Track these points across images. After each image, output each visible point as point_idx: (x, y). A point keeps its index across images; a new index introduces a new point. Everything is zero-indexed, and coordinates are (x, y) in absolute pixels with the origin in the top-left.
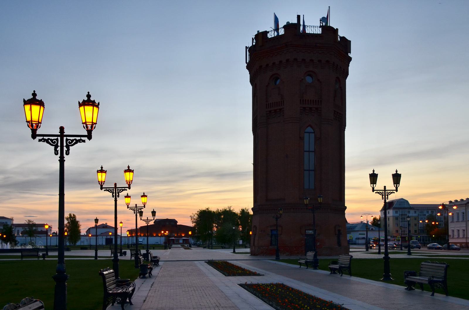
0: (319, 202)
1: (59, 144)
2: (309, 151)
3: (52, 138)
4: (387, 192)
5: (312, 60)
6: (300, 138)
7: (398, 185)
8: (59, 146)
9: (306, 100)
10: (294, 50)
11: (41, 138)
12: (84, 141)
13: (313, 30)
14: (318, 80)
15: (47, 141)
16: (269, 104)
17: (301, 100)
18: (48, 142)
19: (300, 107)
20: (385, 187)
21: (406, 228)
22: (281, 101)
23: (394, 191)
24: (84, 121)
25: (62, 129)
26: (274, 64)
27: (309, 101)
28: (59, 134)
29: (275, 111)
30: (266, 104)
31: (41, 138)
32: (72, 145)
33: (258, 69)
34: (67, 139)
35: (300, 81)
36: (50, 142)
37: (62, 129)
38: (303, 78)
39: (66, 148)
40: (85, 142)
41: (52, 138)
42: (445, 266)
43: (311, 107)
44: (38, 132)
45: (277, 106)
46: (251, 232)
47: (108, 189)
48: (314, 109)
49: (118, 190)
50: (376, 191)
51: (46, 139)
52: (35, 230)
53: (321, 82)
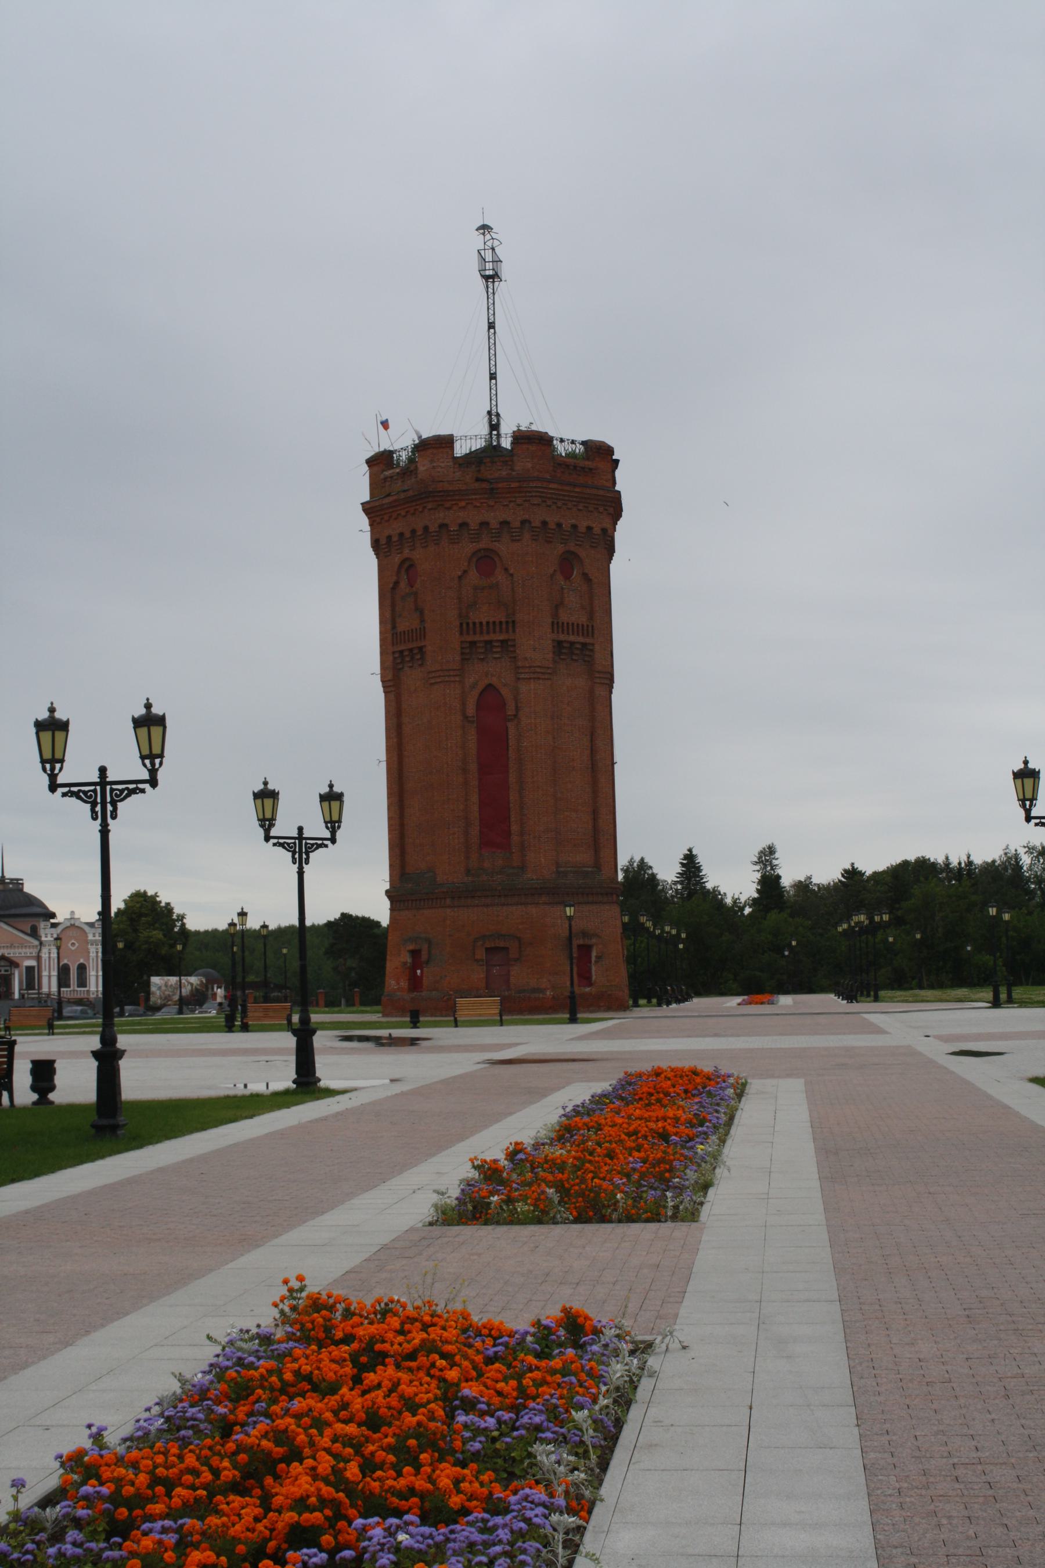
0: (568, 914)
1: (99, 800)
4: (306, 844)
8: (300, 1515)
10: (525, 501)
11: (66, 790)
12: (143, 791)
15: (76, 795)
18: (79, 798)
20: (103, 771)
22: (588, 626)
24: (146, 752)
27: (565, 625)
28: (98, 780)
29: (489, 642)
39: (112, 806)
46: (1007, 919)
48: (578, 646)
49: (112, 790)
50: (275, 841)
51: (74, 791)
53: (512, 575)
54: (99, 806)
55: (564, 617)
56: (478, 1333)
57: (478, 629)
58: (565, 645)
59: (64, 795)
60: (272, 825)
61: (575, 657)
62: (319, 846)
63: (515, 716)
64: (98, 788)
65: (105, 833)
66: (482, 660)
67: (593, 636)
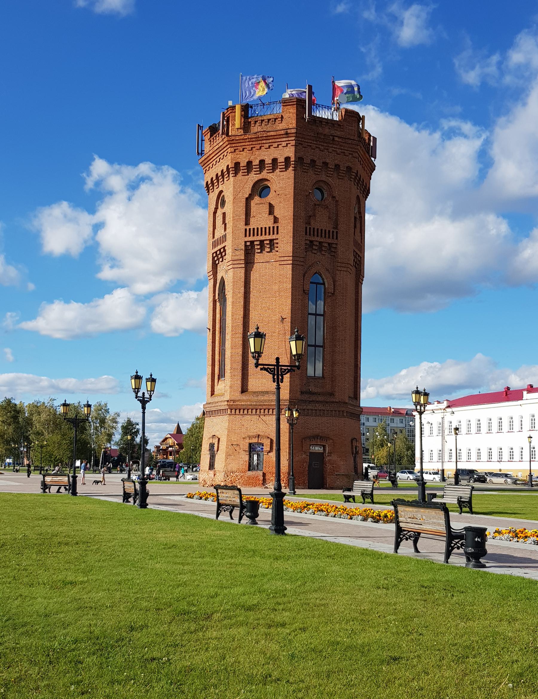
2: (316, 315)
3: (271, 367)
4: (281, 369)
5: (325, 164)
7: (152, 392)
9: (314, 229)
11: (262, 367)
14: (334, 197)
17: (306, 228)
18: (267, 371)
19: (306, 240)
22: (273, 227)
25: (278, 359)
26: (262, 162)
30: (246, 230)
31: (262, 367)
32: (285, 374)
34: (281, 368)
37: (278, 359)
38: (311, 192)
41: (271, 367)
42: (470, 487)
44: (260, 362)
45: (265, 234)
47: (266, 367)
48: (326, 245)
52: (147, 476)
53: (337, 201)
55: (315, 225)
58: (315, 243)
59: (261, 369)
60: (259, 356)
61: (323, 253)
63: (333, 294)
64: (276, 367)
65: (278, 385)
66: (315, 253)
67: (337, 238)
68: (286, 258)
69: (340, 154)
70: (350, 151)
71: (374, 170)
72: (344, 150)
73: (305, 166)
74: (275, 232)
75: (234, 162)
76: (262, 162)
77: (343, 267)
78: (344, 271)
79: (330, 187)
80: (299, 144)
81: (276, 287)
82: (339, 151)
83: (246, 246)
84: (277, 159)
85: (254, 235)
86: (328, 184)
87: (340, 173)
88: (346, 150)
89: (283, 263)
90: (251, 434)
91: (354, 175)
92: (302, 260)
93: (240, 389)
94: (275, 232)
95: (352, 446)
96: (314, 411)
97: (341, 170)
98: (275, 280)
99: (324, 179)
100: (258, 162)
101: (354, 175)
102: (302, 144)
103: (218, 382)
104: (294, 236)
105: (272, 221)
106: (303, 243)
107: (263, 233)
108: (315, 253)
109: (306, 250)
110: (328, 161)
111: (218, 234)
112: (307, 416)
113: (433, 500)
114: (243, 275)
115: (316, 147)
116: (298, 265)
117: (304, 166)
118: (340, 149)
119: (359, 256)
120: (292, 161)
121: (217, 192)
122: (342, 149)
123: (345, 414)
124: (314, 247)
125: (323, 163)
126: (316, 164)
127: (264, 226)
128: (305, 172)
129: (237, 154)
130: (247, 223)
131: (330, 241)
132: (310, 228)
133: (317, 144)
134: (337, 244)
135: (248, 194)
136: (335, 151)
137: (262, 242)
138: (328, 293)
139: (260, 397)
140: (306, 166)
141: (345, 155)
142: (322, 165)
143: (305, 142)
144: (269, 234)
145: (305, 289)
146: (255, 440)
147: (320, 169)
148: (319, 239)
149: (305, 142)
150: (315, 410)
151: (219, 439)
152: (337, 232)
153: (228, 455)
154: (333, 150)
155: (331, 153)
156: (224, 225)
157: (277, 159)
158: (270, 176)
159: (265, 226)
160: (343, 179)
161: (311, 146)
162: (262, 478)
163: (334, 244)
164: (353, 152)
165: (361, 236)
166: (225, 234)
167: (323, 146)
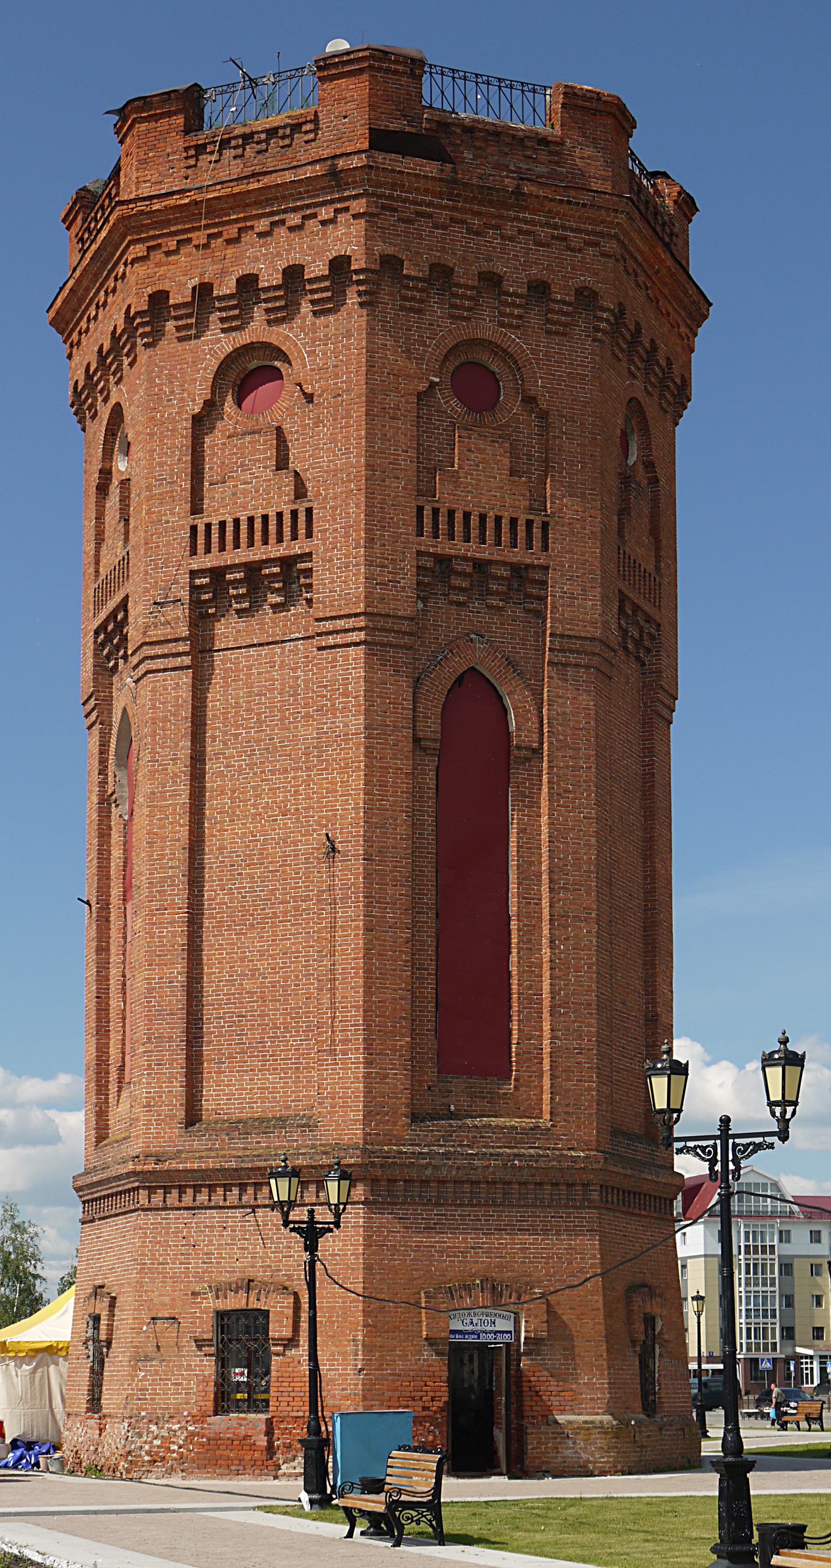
1: (719, 1158)
4: (735, 1145)
6: (416, 740)
7: (790, 1109)
12: (771, 1146)
13: (448, 93)
16: (208, 526)
17: (420, 509)
19: (419, 553)
21: (773, 1284)
22: (294, 514)
23: (769, 1140)
24: (776, 1096)
26: (248, 283)
28: (719, 1133)
30: (194, 529)
33: (139, 314)
34: (734, 1143)
35: (419, 395)
36: (700, 1153)
37: (725, 1121)
38: (437, 380)
39: (734, 1164)
40: (773, 1148)
43: (486, 555)
45: (265, 542)
47: (691, 1144)
48: (505, 573)
53: (543, 415)
54: (719, 1164)
56: (93, 1395)
57: (458, 528)
62: (758, 1147)
64: (718, 1142)
66: (459, 604)
67: (545, 548)
68: (340, 624)
69: (549, 246)
70: (588, 233)
71: (705, 317)
72: (564, 228)
73: (411, 289)
74: (302, 531)
75: (149, 290)
76: (248, 283)
77: (572, 652)
78: (577, 665)
79: (516, 362)
80: (384, 207)
81: (307, 733)
82: (543, 233)
83: (195, 589)
84: (302, 267)
85: (222, 548)
86: (505, 351)
87: (553, 311)
88: (573, 230)
89: (331, 640)
90: (225, 1278)
91: (607, 320)
92: (405, 626)
93: (181, 1114)
94: (302, 531)
95: (630, 1312)
96: (467, 1188)
97: (557, 302)
98: (307, 705)
99: (488, 335)
100: (233, 283)
101: (607, 320)
102: (395, 210)
103: (119, 1091)
104: (370, 541)
105: (290, 489)
106: (409, 565)
107: (258, 535)
108: (459, 604)
109: (423, 592)
110: (500, 268)
111: (108, 561)
112: (438, 1204)
113: (776, 1560)
114: (186, 694)
115: (453, 220)
116: (391, 645)
117: (407, 287)
118: (548, 225)
119: (649, 619)
120: (357, 272)
121: (105, 412)
122: (555, 227)
123: (595, 1196)
124: (456, 581)
125: (482, 276)
126: (456, 279)
127: (261, 512)
128: (411, 310)
129: (158, 265)
130: (196, 509)
131: (518, 555)
132: (436, 512)
133: (455, 209)
134: (547, 568)
135: (200, 402)
136: (528, 233)
137: (252, 569)
138: (518, 748)
139: (253, 1139)
140: (415, 288)
141: (569, 248)
142: (476, 283)
143: (405, 201)
144: (280, 540)
145: (421, 734)
146: (234, 1302)
147: (471, 298)
148: (473, 550)
149: (405, 201)
150: (473, 1183)
151: (114, 1299)
152: (545, 526)
153: (139, 1359)
154: (520, 231)
155: (512, 239)
156: (122, 523)
157: (302, 267)
158: (277, 335)
159: (264, 512)
160: (564, 334)
161: (430, 216)
162: (262, 1441)
163: (534, 567)
164: (601, 234)
165: (658, 549)
166: (124, 553)
167: (478, 214)
